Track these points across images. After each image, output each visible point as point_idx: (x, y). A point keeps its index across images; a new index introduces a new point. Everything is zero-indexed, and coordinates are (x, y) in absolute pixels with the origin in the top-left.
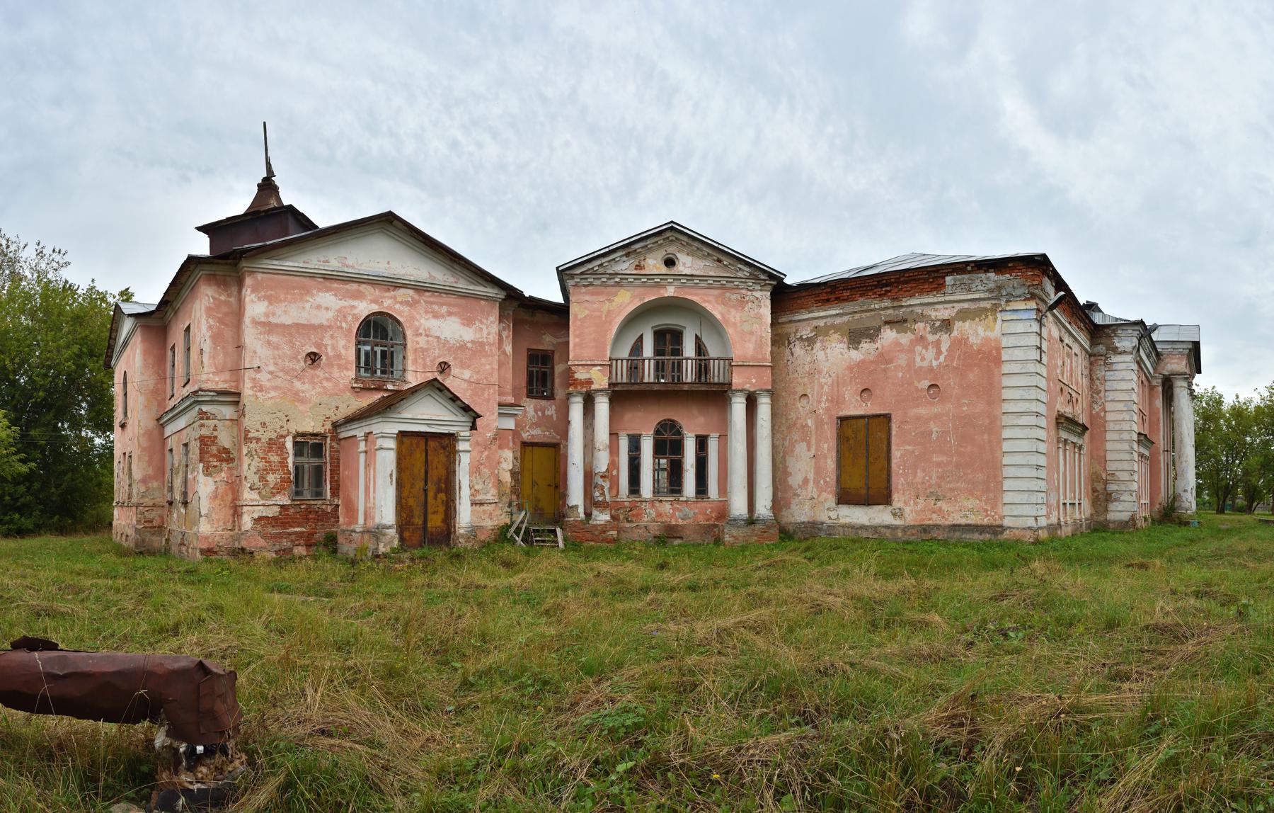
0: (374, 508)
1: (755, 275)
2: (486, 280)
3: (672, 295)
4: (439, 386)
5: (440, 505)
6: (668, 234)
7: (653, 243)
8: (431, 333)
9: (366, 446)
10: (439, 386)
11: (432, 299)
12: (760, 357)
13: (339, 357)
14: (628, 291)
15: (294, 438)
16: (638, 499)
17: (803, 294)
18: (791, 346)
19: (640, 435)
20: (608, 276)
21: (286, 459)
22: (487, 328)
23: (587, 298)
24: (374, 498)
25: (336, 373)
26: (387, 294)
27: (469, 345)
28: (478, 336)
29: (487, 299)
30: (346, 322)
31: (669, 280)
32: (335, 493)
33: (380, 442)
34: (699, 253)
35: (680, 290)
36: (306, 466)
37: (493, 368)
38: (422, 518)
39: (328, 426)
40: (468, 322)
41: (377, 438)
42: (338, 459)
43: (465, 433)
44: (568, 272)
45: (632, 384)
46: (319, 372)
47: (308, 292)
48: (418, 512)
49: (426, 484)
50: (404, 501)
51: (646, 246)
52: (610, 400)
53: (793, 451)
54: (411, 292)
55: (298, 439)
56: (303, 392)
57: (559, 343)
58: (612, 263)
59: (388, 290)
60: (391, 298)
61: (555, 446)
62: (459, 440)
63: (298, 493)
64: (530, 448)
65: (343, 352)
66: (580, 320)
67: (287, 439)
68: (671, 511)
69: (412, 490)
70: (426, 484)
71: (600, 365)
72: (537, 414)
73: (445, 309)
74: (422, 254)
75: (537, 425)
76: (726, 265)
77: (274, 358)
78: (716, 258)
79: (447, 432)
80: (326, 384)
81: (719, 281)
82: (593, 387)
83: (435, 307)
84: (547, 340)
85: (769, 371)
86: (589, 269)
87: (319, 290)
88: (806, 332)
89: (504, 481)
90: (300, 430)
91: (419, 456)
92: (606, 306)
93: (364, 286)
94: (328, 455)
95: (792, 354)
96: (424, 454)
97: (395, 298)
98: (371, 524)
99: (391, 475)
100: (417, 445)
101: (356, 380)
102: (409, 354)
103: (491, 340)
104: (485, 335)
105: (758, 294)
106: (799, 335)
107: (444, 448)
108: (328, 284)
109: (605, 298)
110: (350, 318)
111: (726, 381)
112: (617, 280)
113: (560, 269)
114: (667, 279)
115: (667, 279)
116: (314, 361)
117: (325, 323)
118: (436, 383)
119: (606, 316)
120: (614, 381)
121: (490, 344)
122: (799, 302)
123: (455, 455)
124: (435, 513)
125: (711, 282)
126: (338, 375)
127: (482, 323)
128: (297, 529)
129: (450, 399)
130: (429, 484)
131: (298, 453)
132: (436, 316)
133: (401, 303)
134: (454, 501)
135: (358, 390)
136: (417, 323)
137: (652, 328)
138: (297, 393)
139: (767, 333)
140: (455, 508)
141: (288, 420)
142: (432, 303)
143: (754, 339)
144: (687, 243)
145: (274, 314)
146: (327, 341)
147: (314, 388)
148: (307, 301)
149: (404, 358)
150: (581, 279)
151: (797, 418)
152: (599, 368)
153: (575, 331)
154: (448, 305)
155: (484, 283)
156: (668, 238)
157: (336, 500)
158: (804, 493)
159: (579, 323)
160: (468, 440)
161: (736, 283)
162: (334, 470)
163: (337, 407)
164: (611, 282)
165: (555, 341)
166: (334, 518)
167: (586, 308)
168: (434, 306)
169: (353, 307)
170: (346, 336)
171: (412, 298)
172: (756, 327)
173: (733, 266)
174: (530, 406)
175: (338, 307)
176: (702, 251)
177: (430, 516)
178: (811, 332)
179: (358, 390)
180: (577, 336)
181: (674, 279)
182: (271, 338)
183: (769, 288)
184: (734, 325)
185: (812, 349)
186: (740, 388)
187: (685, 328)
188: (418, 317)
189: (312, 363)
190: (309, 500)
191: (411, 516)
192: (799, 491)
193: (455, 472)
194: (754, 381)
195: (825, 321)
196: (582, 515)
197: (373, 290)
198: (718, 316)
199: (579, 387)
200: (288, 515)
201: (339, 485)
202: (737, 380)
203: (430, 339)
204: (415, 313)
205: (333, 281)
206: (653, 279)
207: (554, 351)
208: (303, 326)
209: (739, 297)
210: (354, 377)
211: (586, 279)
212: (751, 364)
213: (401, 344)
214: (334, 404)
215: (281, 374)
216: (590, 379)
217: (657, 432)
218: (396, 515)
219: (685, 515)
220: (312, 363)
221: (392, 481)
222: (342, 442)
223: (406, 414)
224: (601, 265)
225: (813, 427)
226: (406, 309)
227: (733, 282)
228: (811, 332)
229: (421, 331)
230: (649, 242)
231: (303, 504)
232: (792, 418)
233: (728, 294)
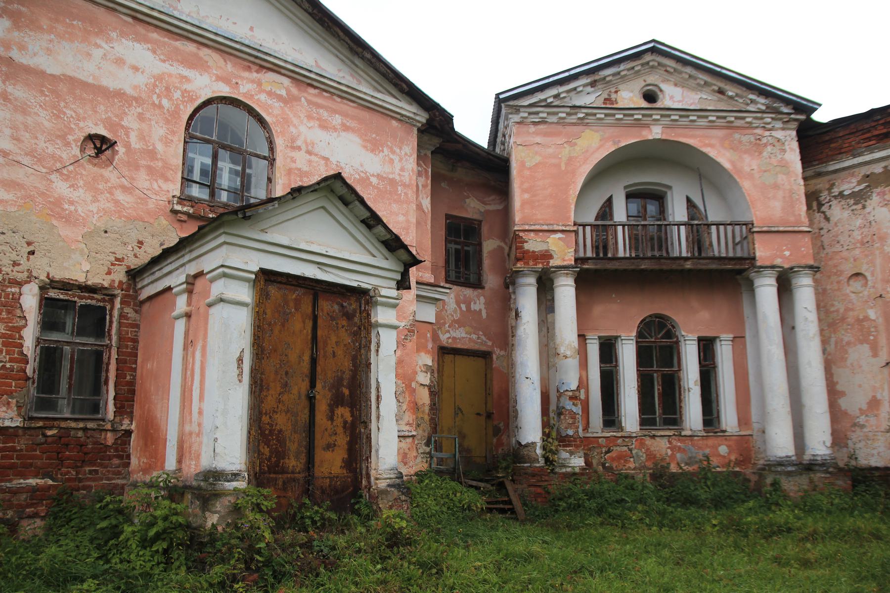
0: (198, 435)
1: (775, 108)
2: (402, 91)
3: (658, 137)
4: (343, 191)
5: (340, 430)
6: (648, 57)
7: (628, 70)
8: (316, 150)
9: (189, 303)
10: (343, 191)
11: (319, 101)
12: (792, 219)
13: (152, 154)
14: (597, 131)
15: (42, 288)
16: (619, 434)
17: (841, 134)
18: (823, 209)
19: (616, 338)
20: (568, 110)
21: (19, 329)
22: (401, 160)
23: (538, 139)
24: (200, 413)
25: (143, 180)
26: (246, 74)
27: (374, 180)
28: (387, 169)
29: (402, 119)
30: (170, 99)
31: (654, 117)
32: (125, 404)
33: (218, 288)
34: (692, 82)
35: (669, 130)
36: (67, 348)
37: (408, 221)
38: (303, 459)
39: (120, 275)
40: (374, 147)
41: (212, 281)
42: (135, 341)
43: (388, 291)
44: (511, 103)
45: (610, 259)
46: (108, 173)
47: (101, 32)
48: (294, 444)
49: (313, 385)
50: (265, 419)
51: (619, 73)
52: (576, 281)
53: (844, 359)
54: (286, 81)
55: (53, 294)
56: (71, 203)
57: (487, 212)
58: (572, 94)
59: (249, 69)
60: (253, 82)
61: (485, 355)
62: (376, 304)
63: (45, 404)
64: (451, 356)
65: (160, 147)
66: (530, 168)
67: (26, 288)
68: (669, 452)
69: (285, 397)
70: (313, 385)
71: (562, 231)
72: (460, 308)
73: (337, 120)
74: (306, 32)
75: (459, 323)
76: (731, 98)
77: (14, 128)
78: (716, 88)
79: (355, 284)
80: (120, 196)
81: (725, 118)
82: (552, 263)
83: (325, 114)
84: (472, 205)
85: (807, 239)
86: (541, 101)
87: (123, 34)
88: (849, 185)
89: (420, 403)
90: (58, 275)
91: (300, 326)
92: (566, 151)
93: (206, 51)
94: (114, 331)
95: (827, 219)
96: (309, 324)
97: (259, 83)
98: (191, 469)
99: (240, 360)
100: (297, 302)
101: (182, 200)
102: (278, 175)
103: (406, 180)
104: (397, 171)
105: (779, 134)
106: (836, 191)
107: (349, 316)
108: (141, 29)
109: (564, 140)
110: (177, 95)
111: (746, 255)
112: (581, 115)
113: (501, 97)
114: (651, 116)
115: (651, 116)
116: (99, 151)
117: (129, 91)
118: (338, 185)
119: (567, 164)
120: (581, 255)
121: (404, 185)
122: (832, 145)
123: (369, 333)
124: (330, 447)
125: (714, 118)
126: (146, 184)
127: (393, 152)
128: (32, 482)
129: (363, 222)
130: (319, 386)
131: (49, 322)
132: (324, 126)
133: (270, 94)
134: (366, 424)
135: (184, 218)
136: (292, 129)
137: (625, 187)
138: (58, 202)
139: (800, 188)
140: (369, 438)
141: (32, 253)
142: (319, 106)
143: (780, 194)
144: (675, 70)
145: (22, 48)
146: (130, 121)
147: (95, 200)
148: (98, 46)
149: (270, 180)
150: (530, 114)
151: (847, 310)
152: (560, 235)
153: (522, 183)
154: (345, 115)
155: (394, 92)
156: (648, 63)
157: (126, 422)
158: (873, 421)
159: (527, 173)
160: (394, 306)
161: (748, 120)
162: (125, 362)
163: (141, 243)
164: (573, 119)
165: (482, 208)
166: (120, 457)
167: (536, 153)
168: (321, 111)
169: (187, 79)
170: (168, 122)
171: (288, 91)
172: (781, 178)
173: (741, 97)
174: (451, 296)
175: (157, 71)
176: (696, 78)
177: (320, 455)
178: (859, 183)
179: (184, 218)
180: (524, 191)
181: (662, 116)
182: (10, 89)
183: (795, 125)
184: (750, 176)
185: (864, 207)
186: (768, 263)
187: (670, 187)
188: (295, 121)
189: (97, 155)
190: (66, 419)
191: (280, 454)
192: (862, 420)
193: (368, 365)
194: (787, 253)
195: (883, 164)
196: (542, 462)
197: (222, 61)
198: (727, 165)
199: (531, 263)
200: (13, 449)
201: (133, 392)
202: (763, 252)
203: (313, 158)
204: (291, 115)
205: (151, 28)
206: (632, 115)
207: (480, 222)
208: (85, 85)
209: (752, 139)
210: (178, 194)
211: (537, 113)
212: (781, 229)
213: (265, 158)
214: (135, 236)
215: (26, 160)
216: (547, 251)
217: (640, 335)
218: (249, 450)
219: (690, 458)
220: (97, 155)
221: (241, 374)
222: (146, 307)
223: (275, 236)
224: (556, 96)
225: (881, 320)
226: (277, 104)
227: (744, 118)
228: (859, 183)
229: (299, 143)
230: (622, 67)
231: (51, 428)
232: (837, 311)
233: (737, 136)
